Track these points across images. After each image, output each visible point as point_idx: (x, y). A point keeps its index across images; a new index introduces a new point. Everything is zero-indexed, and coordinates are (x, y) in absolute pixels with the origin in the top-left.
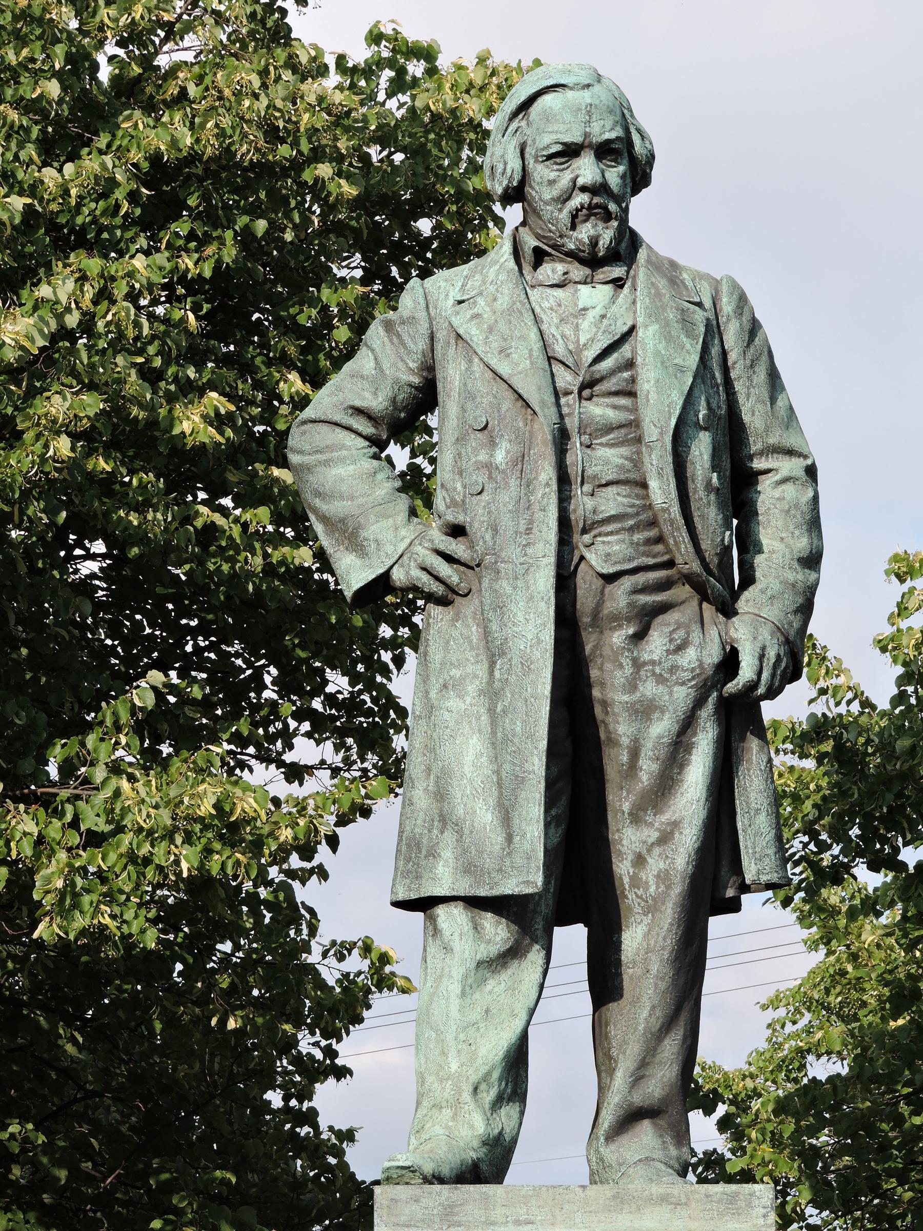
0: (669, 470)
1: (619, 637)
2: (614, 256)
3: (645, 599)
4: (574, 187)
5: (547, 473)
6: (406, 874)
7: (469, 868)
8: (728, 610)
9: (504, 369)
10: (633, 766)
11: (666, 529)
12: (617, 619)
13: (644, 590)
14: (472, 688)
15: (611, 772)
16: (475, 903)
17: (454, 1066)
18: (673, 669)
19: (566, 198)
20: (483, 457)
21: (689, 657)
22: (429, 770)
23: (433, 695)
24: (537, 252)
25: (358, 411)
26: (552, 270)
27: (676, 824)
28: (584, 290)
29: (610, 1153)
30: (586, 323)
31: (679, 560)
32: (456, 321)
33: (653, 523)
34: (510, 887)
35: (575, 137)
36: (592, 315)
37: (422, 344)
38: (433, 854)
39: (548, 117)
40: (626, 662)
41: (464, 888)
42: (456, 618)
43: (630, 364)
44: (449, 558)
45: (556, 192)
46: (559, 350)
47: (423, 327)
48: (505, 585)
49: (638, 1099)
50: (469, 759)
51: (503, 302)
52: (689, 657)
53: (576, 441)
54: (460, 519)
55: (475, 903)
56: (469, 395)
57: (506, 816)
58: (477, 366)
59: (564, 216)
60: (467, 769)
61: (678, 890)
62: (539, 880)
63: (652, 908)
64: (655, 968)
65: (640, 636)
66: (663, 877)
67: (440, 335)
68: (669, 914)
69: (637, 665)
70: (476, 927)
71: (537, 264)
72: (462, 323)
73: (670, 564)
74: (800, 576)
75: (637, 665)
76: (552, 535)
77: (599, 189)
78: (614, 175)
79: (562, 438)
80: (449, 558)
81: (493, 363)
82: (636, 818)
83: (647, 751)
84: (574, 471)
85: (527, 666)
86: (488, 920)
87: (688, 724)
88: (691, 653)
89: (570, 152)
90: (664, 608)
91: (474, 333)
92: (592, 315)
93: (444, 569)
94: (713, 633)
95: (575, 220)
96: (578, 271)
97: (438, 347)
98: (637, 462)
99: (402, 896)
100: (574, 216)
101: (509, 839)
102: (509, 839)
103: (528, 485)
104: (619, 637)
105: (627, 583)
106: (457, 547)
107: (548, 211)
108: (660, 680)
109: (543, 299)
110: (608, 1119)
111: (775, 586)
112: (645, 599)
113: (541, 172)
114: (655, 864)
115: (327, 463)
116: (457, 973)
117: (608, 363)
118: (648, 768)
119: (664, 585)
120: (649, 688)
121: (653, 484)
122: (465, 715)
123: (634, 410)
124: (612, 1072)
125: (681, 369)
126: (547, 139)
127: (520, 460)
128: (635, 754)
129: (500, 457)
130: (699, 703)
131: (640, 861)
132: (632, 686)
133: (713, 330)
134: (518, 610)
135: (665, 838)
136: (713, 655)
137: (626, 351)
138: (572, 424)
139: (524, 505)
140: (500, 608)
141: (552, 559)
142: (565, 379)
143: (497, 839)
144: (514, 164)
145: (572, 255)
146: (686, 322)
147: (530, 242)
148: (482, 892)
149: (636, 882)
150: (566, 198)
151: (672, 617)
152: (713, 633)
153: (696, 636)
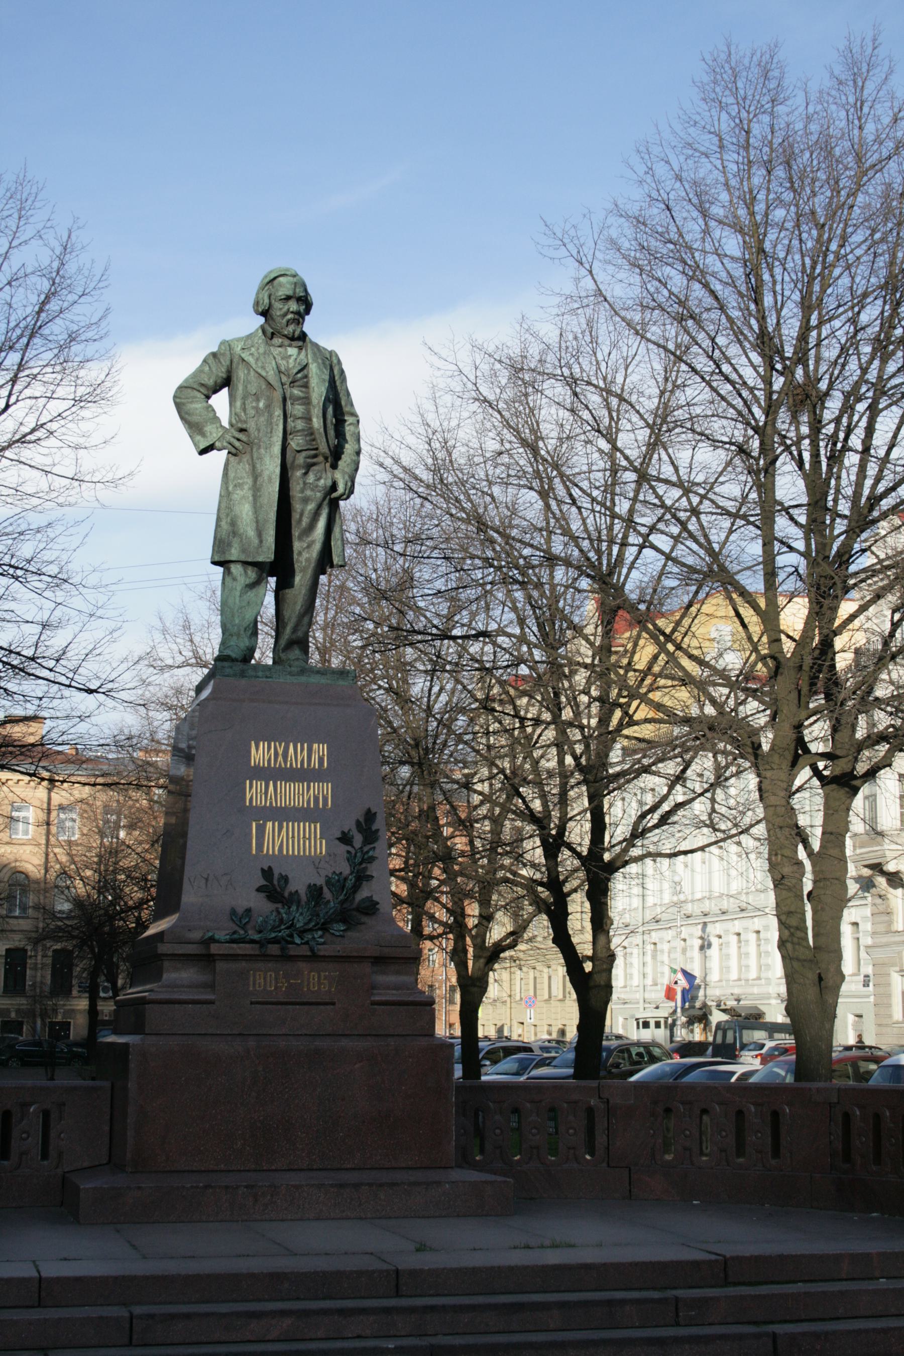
0: (321, 415)
1: (299, 473)
2: (299, 339)
3: (309, 460)
4: (288, 312)
5: (278, 412)
6: (218, 552)
7: (244, 551)
8: (334, 466)
9: (264, 374)
10: (300, 520)
11: (317, 436)
12: (300, 467)
13: (309, 457)
14: (246, 487)
15: (294, 523)
16: (245, 563)
17: (237, 621)
18: (317, 486)
19: (285, 314)
20: (254, 404)
21: (322, 482)
22: (227, 515)
23: (230, 489)
24: (273, 334)
25: (202, 385)
26: (277, 341)
27: (313, 542)
28: (289, 349)
30: (291, 361)
31: (321, 448)
32: (243, 355)
33: (312, 434)
34: (260, 559)
35: (290, 293)
36: (293, 358)
37: (228, 363)
39: (281, 285)
40: (301, 482)
41: (243, 558)
43: (306, 377)
44: (238, 440)
45: (282, 312)
46: (283, 369)
48: (262, 451)
49: (294, 637)
52: (322, 482)
53: (289, 403)
54: (244, 426)
55: (245, 563)
57: (260, 534)
58: (252, 373)
59: (284, 321)
60: (244, 516)
61: (313, 565)
62: (273, 557)
63: (304, 570)
64: (303, 592)
65: (306, 474)
66: (308, 560)
67: (235, 360)
68: (310, 572)
70: (246, 572)
71: (271, 338)
72: (245, 355)
73: (317, 449)
74: (355, 458)
75: (305, 483)
76: (281, 435)
77: (298, 313)
78: (302, 308)
79: (284, 400)
80: (238, 440)
81: (260, 371)
82: (300, 538)
83: (306, 514)
84: (289, 412)
85: (270, 479)
87: (319, 507)
88: (322, 482)
89: (288, 298)
90: (314, 464)
91: (251, 360)
92: (293, 358)
93: (237, 444)
95: (288, 323)
96: (287, 342)
97: (234, 365)
98: (308, 412)
100: (288, 321)
101: (261, 541)
102: (261, 541)
103: (271, 416)
104: (299, 473)
105: (304, 454)
106: (241, 436)
107: (278, 319)
108: (312, 490)
109: (276, 351)
111: (349, 461)
112: (309, 460)
113: (277, 305)
114: (305, 555)
115: (191, 402)
116: (239, 588)
117: (299, 375)
118: (305, 521)
119: (315, 456)
120: (308, 493)
121: (315, 420)
122: (243, 497)
123: (308, 393)
124: (284, 628)
125: (324, 380)
126: (280, 293)
127: (268, 406)
128: (302, 515)
129: (261, 405)
131: (300, 553)
132: (302, 491)
133: (332, 370)
134: (267, 460)
135: (309, 547)
137: (305, 371)
138: (288, 396)
139: (270, 423)
141: (280, 443)
142: (284, 379)
143: (256, 541)
144: (267, 301)
145: (286, 336)
146: (324, 363)
147: (269, 330)
148: (250, 560)
149: (298, 561)
150: (285, 314)
153: (324, 476)
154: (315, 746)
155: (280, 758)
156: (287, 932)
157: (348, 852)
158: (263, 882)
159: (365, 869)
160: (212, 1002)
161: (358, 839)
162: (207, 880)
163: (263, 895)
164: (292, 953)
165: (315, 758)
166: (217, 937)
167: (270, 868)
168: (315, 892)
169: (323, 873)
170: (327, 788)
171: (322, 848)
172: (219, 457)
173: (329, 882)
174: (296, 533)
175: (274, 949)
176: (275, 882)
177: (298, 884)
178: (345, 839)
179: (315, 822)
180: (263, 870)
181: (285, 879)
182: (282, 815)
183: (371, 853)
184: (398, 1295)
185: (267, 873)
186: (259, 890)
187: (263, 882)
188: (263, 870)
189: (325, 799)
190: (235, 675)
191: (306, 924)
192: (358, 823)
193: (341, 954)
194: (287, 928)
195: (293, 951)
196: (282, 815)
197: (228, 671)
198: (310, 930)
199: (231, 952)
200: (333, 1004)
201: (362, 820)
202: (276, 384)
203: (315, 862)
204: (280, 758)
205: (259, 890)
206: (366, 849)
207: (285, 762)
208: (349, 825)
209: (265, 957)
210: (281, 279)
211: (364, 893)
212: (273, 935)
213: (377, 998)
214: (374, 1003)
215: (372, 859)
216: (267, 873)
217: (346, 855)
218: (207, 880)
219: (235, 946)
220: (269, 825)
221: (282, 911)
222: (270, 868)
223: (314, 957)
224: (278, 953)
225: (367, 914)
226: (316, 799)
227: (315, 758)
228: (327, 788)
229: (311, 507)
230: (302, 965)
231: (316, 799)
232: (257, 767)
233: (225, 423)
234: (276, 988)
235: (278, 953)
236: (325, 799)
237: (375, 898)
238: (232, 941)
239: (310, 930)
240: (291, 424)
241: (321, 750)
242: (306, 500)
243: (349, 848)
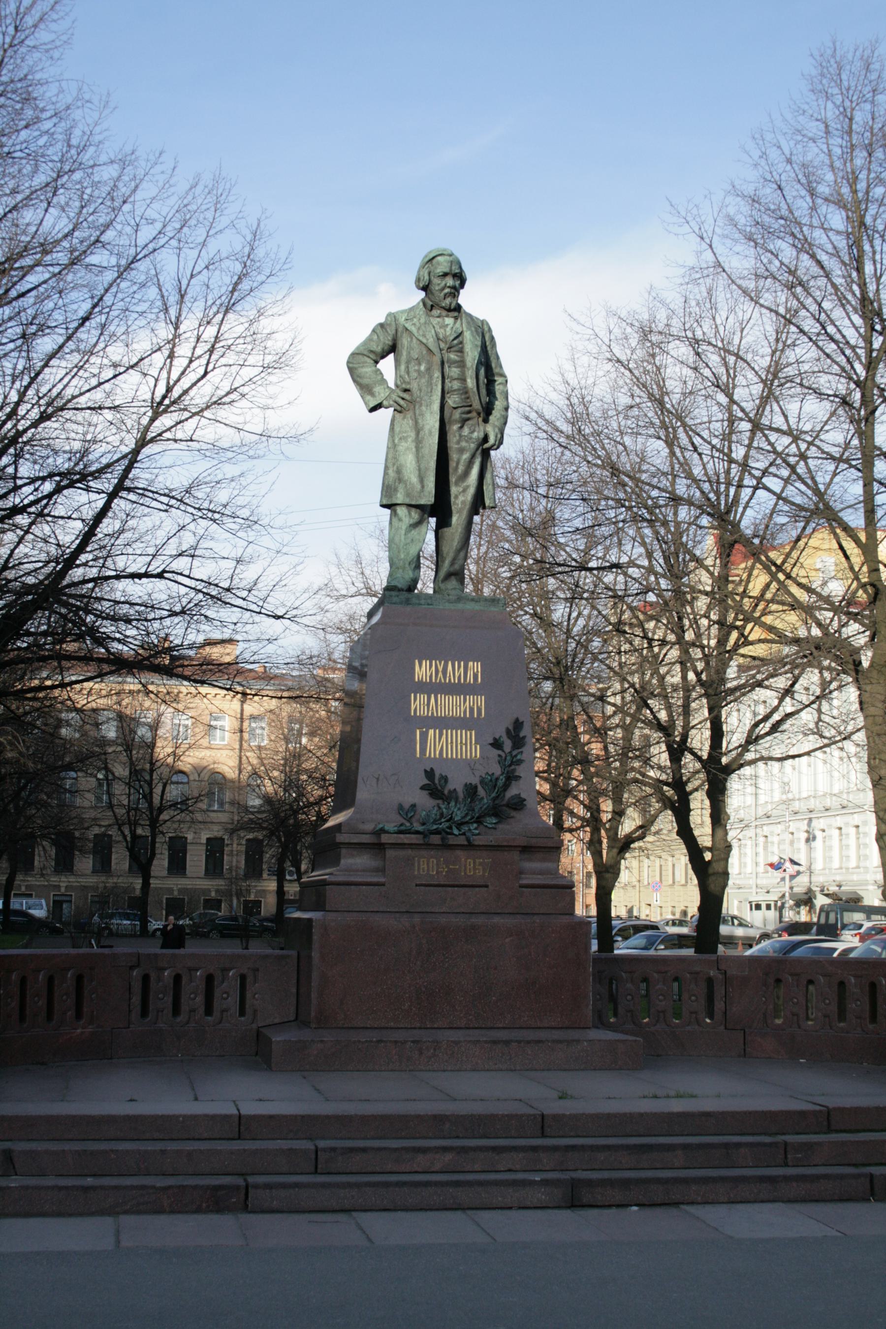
4: (445, 287)
5: (437, 374)
7: (408, 495)
8: (486, 421)
9: (424, 341)
10: (457, 468)
14: (410, 440)
15: (451, 470)
16: (410, 506)
19: (443, 289)
21: (475, 435)
23: (396, 441)
25: (372, 351)
26: (436, 312)
29: (442, 586)
30: (448, 329)
33: (466, 393)
38: (396, 490)
39: (438, 263)
41: (407, 501)
42: (404, 418)
43: (461, 343)
46: (441, 336)
47: (394, 328)
48: (424, 408)
49: (452, 569)
50: (409, 461)
51: (422, 320)
53: (446, 366)
54: (408, 387)
55: (410, 506)
56: (410, 348)
57: (422, 480)
58: (414, 340)
59: (442, 294)
61: (468, 507)
63: (460, 511)
65: (461, 427)
66: (463, 502)
67: (400, 330)
68: (465, 513)
69: (460, 436)
75: (460, 436)
76: (439, 394)
78: (458, 283)
79: (443, 363)
82: (457, 484)
83: (462, 462)
84: (446, 374)
85: (430, 433)
86: (413, 510)
87: (473, 456)
89: (445, 275)
90: (468, 419)
91: (413, 329)
93: (402, 402)
94: (482, 428)
96: (444, 313)
99: (385, 502)
101: (423, 487)
102: (423, 487)
103: (431, 377)
104: (455, 427)
105: (459, 410)
106: (405, 396)
107: (437, 293)
108: (467, 441)
109: (435, 321)
110: (442, 574)
113: (436, 281)
114: (461, 498)
116: (404, 527)
118: (461, 468)
120: (464, 444)
121: (469, 380)
122: (407, 449)
123: (463, 357)
127: (428, 369)
128: (458, 463)
129: (423, 368)
130: (477, 449)
131: (456, 497)
132: (458, 442)
134: (428, 416)
135: (464, 491)
136: (482, 435)
138: (445, 360)
139: (430, 384)
140: (422, 415)
142: (442, 345)
143: (419, 487)
144: (427, 277)
147: (429, 303)
148: (413, 503)
150: (443, 289)
151: (470, 422)
152: (482, 428)
154: (471, 664)
155: (440, 675)
156: (447, 824)
157: (500, 756)
158: (426, 782)
159: (514, 770)
160: (383, 885)
161: (508, 745)
162: (378, 779)
163: (425, 793)
164: (451, 842)
165: (470, 674)
166: (386, 828)
167: (432, 769)
168: (471, 791)
169: (478, 774)
170: (480, 701)
171: (476, 752)
172: (386, 414)
173: (482, 781)
174: (453, 479)
175: (436, 839)
176: (437, 781)
177: (457, 783)
178: (497, 744)
179: (471, 730)
180: (426, 771)
181: (445, 779)
182: (443, 723)
183: (519, 757)
184: (543, 1135)
185: (430, 774)
186: (423, 788)
187: (426, 782)
188: (426, 771)
189: (479, 710)
190: (401, 603)
191: (463, 818)
192: (508, 731)
193: (493, 843)
194: (448, 821)
195: (452, 840)
196: (443, 723)
197: (395, 599)
198: (467, 823)
199: (399, 841)
200: (487, 886)
201: (511, 728)
202: (435, 350)
203: (471, 764)
204: (440, 675)
205: (423, 788)
206: (514, 753)
207: (445, 678)
208: (500, 732)
209: (428, 846)
210: (439, 258)
211: (512, 792)
212: (435, 827)
213: (524, 882)
214: (522, 886)
215: (520, 762)
216: (430, 774)
217: (497, 758)
218: (378, 779)
219: (402, 836)
220: (431, 732)
221: (443, 806)
222: (432, 769)
223: (470, 846)
224: (440, 842)
225: (515, 809)
226: (472, 710)
227: (470, 674)
228: (480, 701)
229: (466, 456)
230: (459, 853)
231: (472, 710)
232: (420, 682)
233: (392, 385)
234: (437, 873)
235: (440, 842)
236: (479, 710)
237: (523, 796)
238: (400, 832)
239: (467, 823)
240: (448, 384)
241: (475, 667)
242: (461, 451)
243: (500, 752)
